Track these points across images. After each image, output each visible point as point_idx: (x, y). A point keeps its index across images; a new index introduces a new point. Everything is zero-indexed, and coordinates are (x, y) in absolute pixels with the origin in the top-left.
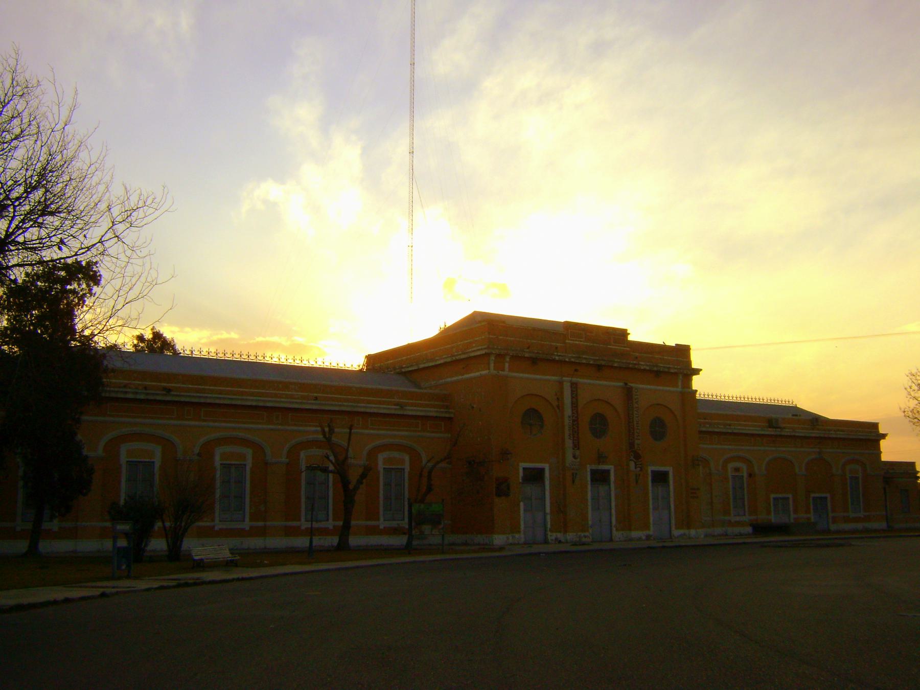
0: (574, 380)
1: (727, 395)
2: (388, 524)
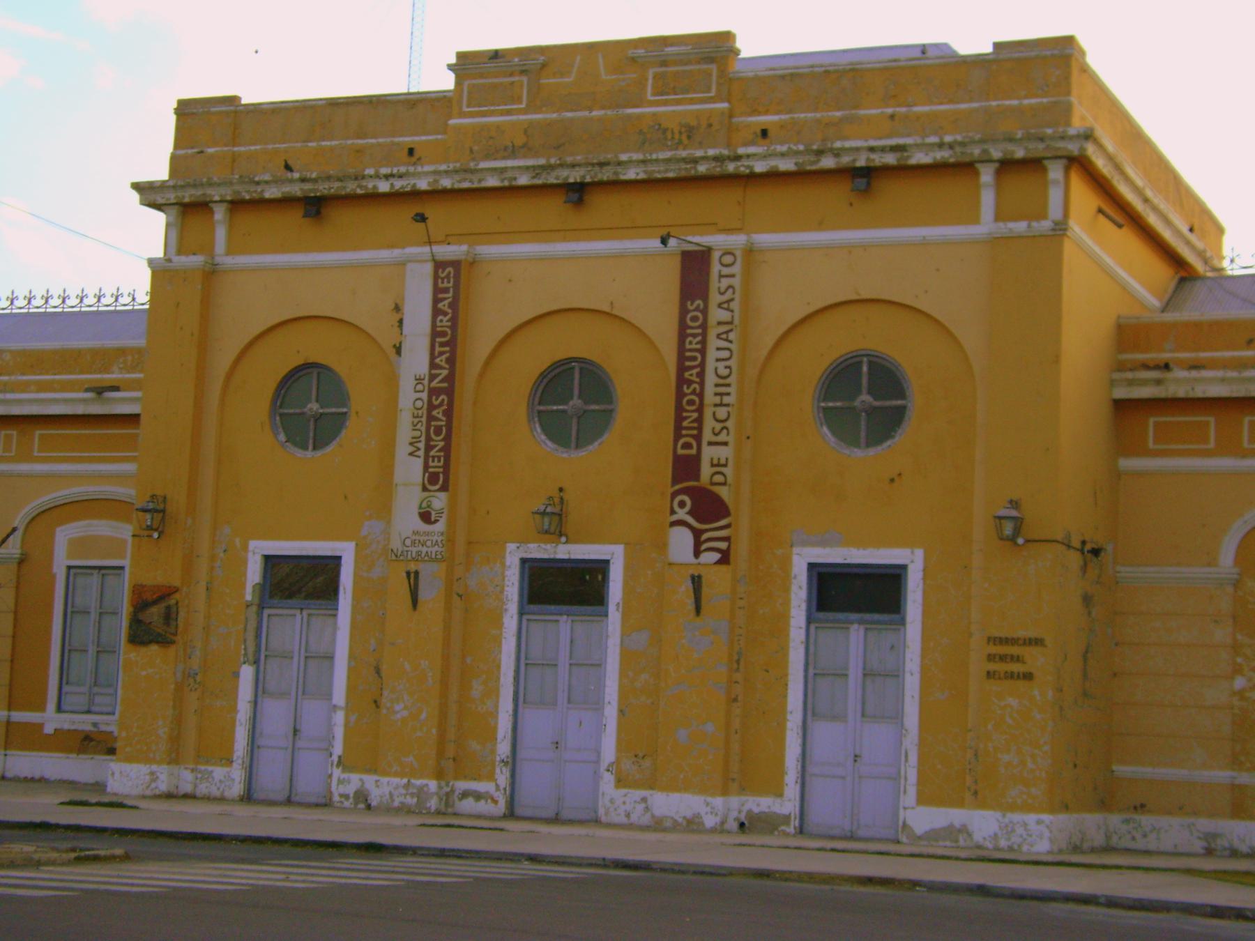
2: (67, 722)
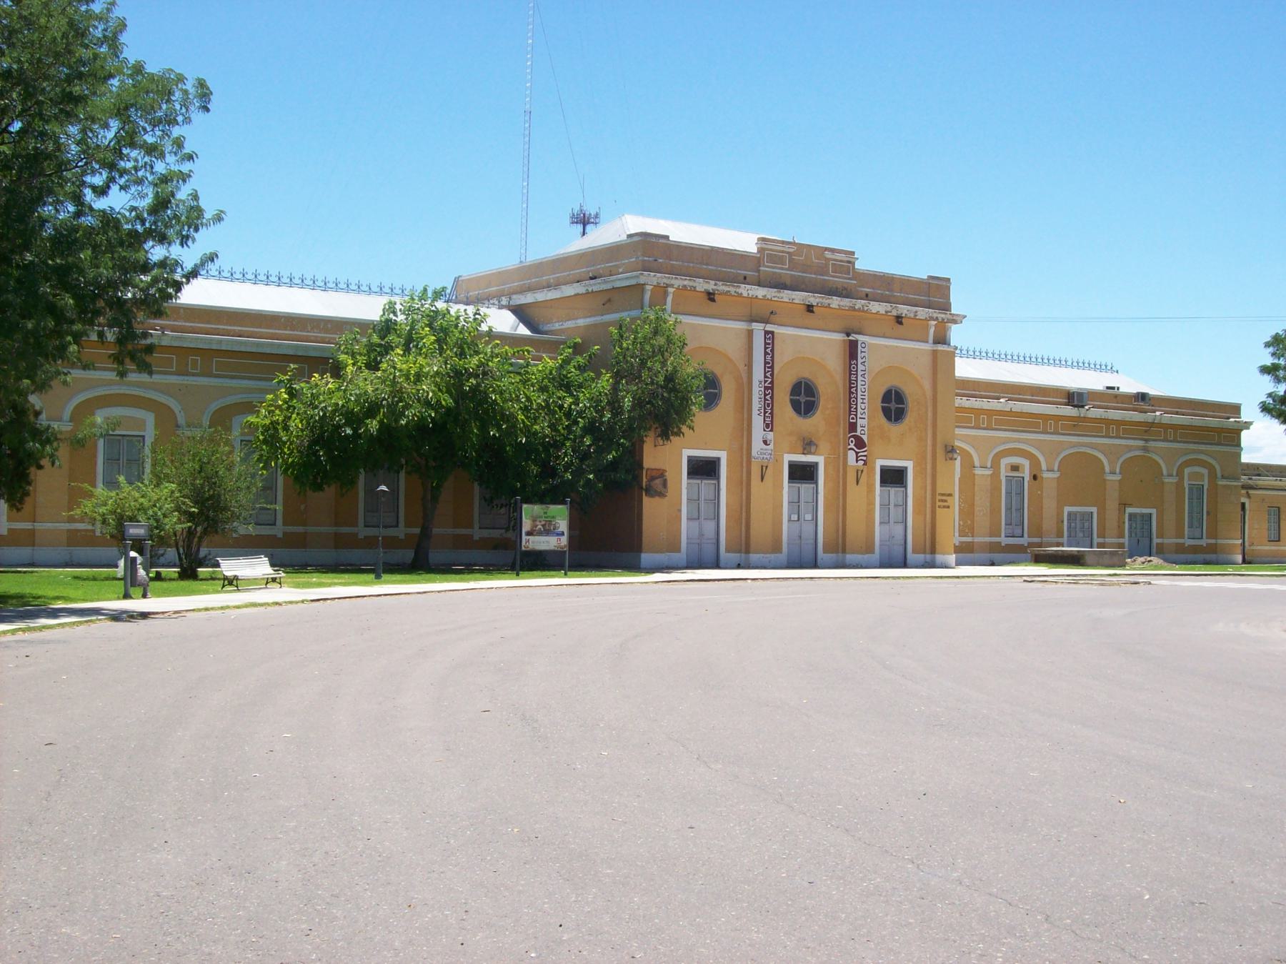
0: (769, 328)
1: (1010, 353)
2: (486, 533)
